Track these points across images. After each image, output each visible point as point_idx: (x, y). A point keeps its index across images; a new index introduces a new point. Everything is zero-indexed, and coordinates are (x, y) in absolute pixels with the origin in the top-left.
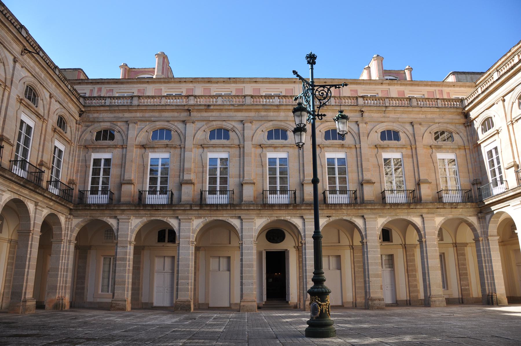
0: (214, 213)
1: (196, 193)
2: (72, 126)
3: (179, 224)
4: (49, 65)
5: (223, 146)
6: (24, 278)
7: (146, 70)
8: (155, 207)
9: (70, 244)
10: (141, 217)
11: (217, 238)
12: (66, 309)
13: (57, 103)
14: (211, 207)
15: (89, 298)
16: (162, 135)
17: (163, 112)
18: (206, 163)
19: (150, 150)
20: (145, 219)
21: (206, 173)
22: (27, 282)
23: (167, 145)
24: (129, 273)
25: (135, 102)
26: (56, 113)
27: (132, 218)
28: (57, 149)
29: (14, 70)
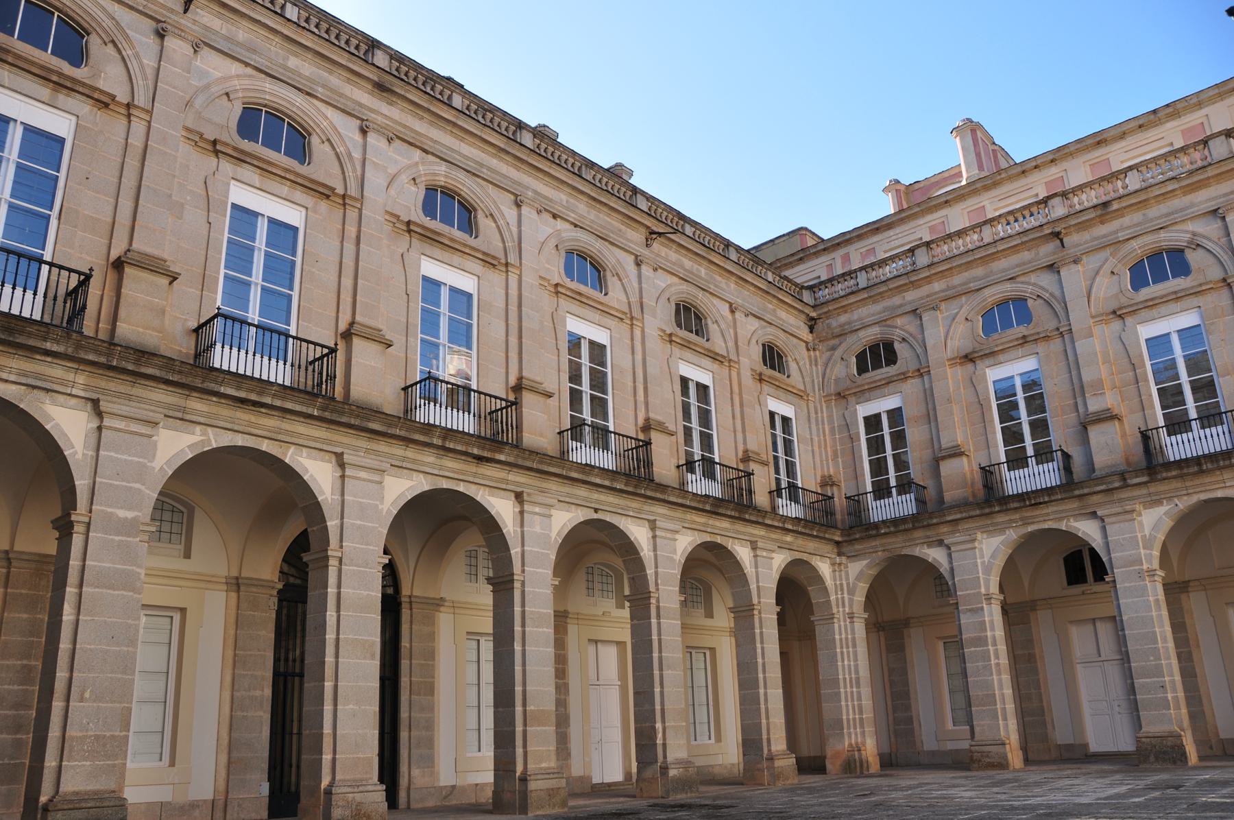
0: (1197, 482)
1: (1130, 440)
2: (798, 359)
3: (1104, 529)
4: (713, 246)
5: (1177, 297)
6: (759, 709)
7: (946, 175)
8: (1029, 499)
9: (852, 622)
10: (1002, 531)
12: (872, 771)
13: (751, 318)
14: (1181, 468)
15: (928, 741)
16: (1008, 314)
17: (994, 260)
18: (1141, 355)
19: (987, 362)
20: (1012, 535)
21: (1147, 380)
22: (767, 718)
23: (1024, 337)
24: (999, 673)
25: (922, 258)
26: (754, 341)
27: (979, 536)
29: (640, 283)
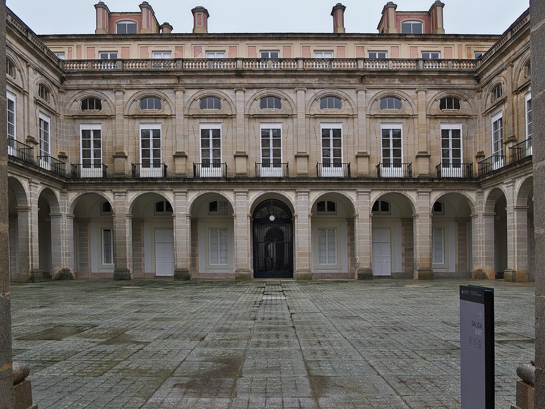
11: (212, 212)
19: (82, 121)
28: (42, 122)
